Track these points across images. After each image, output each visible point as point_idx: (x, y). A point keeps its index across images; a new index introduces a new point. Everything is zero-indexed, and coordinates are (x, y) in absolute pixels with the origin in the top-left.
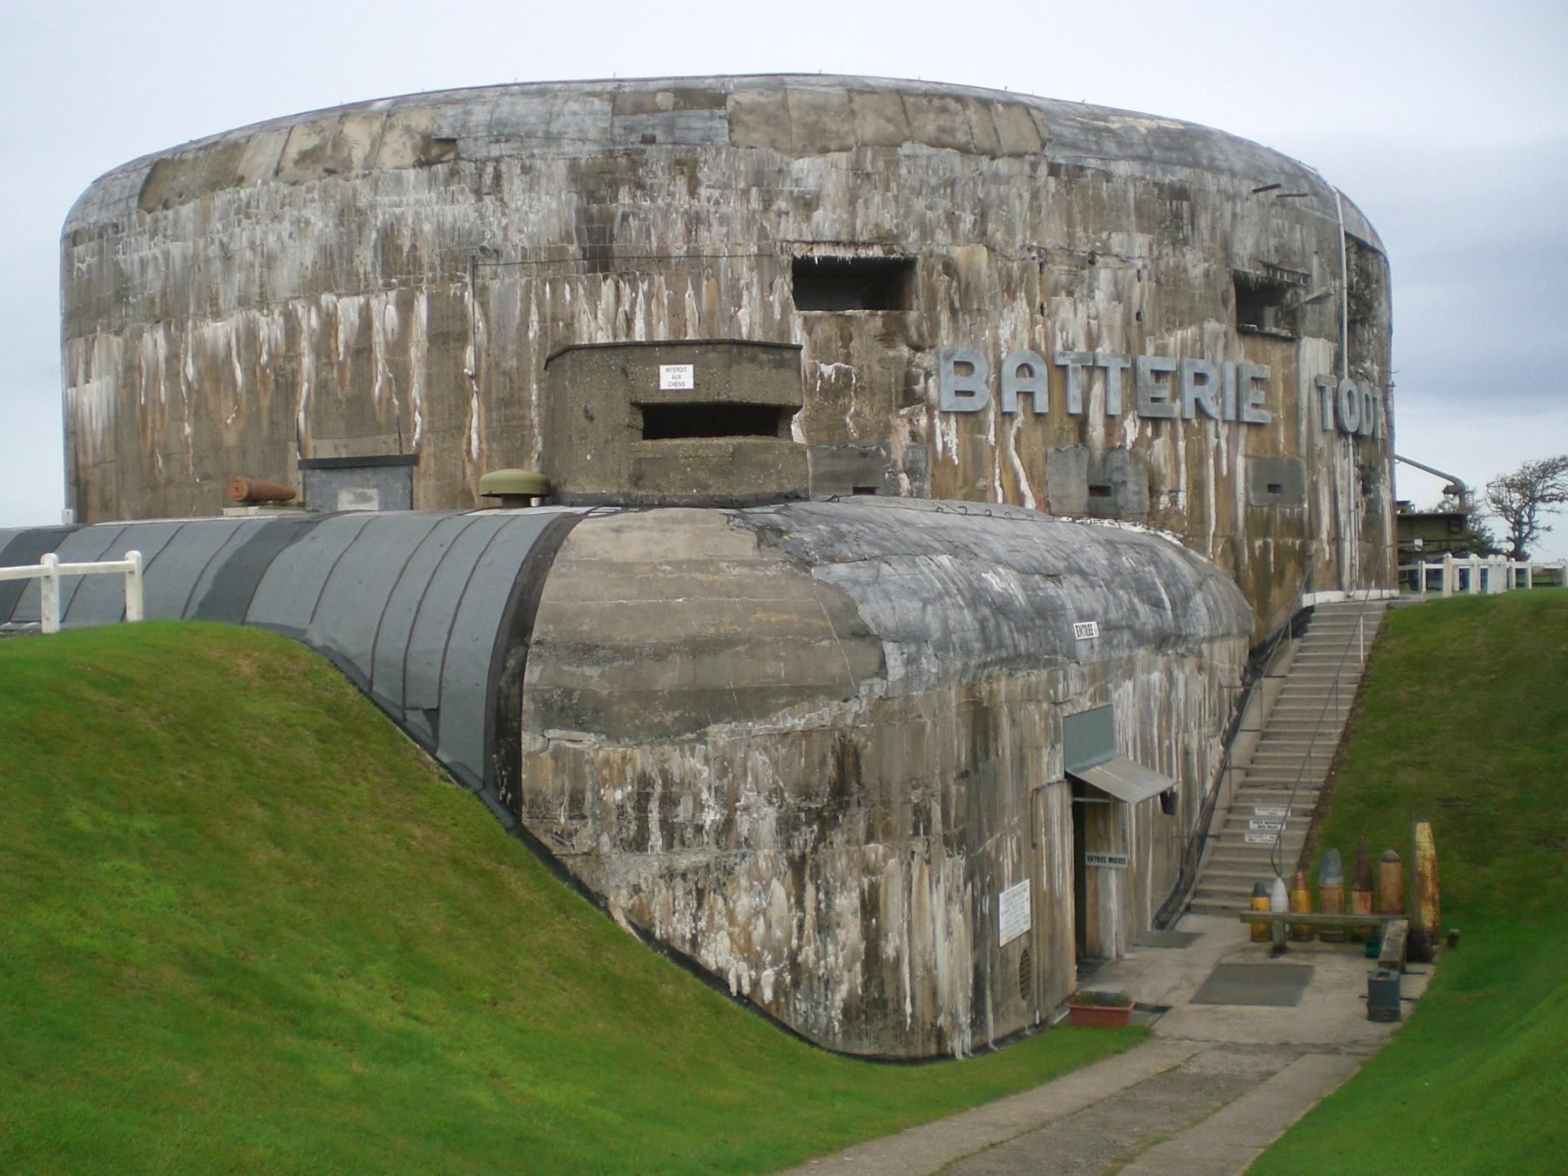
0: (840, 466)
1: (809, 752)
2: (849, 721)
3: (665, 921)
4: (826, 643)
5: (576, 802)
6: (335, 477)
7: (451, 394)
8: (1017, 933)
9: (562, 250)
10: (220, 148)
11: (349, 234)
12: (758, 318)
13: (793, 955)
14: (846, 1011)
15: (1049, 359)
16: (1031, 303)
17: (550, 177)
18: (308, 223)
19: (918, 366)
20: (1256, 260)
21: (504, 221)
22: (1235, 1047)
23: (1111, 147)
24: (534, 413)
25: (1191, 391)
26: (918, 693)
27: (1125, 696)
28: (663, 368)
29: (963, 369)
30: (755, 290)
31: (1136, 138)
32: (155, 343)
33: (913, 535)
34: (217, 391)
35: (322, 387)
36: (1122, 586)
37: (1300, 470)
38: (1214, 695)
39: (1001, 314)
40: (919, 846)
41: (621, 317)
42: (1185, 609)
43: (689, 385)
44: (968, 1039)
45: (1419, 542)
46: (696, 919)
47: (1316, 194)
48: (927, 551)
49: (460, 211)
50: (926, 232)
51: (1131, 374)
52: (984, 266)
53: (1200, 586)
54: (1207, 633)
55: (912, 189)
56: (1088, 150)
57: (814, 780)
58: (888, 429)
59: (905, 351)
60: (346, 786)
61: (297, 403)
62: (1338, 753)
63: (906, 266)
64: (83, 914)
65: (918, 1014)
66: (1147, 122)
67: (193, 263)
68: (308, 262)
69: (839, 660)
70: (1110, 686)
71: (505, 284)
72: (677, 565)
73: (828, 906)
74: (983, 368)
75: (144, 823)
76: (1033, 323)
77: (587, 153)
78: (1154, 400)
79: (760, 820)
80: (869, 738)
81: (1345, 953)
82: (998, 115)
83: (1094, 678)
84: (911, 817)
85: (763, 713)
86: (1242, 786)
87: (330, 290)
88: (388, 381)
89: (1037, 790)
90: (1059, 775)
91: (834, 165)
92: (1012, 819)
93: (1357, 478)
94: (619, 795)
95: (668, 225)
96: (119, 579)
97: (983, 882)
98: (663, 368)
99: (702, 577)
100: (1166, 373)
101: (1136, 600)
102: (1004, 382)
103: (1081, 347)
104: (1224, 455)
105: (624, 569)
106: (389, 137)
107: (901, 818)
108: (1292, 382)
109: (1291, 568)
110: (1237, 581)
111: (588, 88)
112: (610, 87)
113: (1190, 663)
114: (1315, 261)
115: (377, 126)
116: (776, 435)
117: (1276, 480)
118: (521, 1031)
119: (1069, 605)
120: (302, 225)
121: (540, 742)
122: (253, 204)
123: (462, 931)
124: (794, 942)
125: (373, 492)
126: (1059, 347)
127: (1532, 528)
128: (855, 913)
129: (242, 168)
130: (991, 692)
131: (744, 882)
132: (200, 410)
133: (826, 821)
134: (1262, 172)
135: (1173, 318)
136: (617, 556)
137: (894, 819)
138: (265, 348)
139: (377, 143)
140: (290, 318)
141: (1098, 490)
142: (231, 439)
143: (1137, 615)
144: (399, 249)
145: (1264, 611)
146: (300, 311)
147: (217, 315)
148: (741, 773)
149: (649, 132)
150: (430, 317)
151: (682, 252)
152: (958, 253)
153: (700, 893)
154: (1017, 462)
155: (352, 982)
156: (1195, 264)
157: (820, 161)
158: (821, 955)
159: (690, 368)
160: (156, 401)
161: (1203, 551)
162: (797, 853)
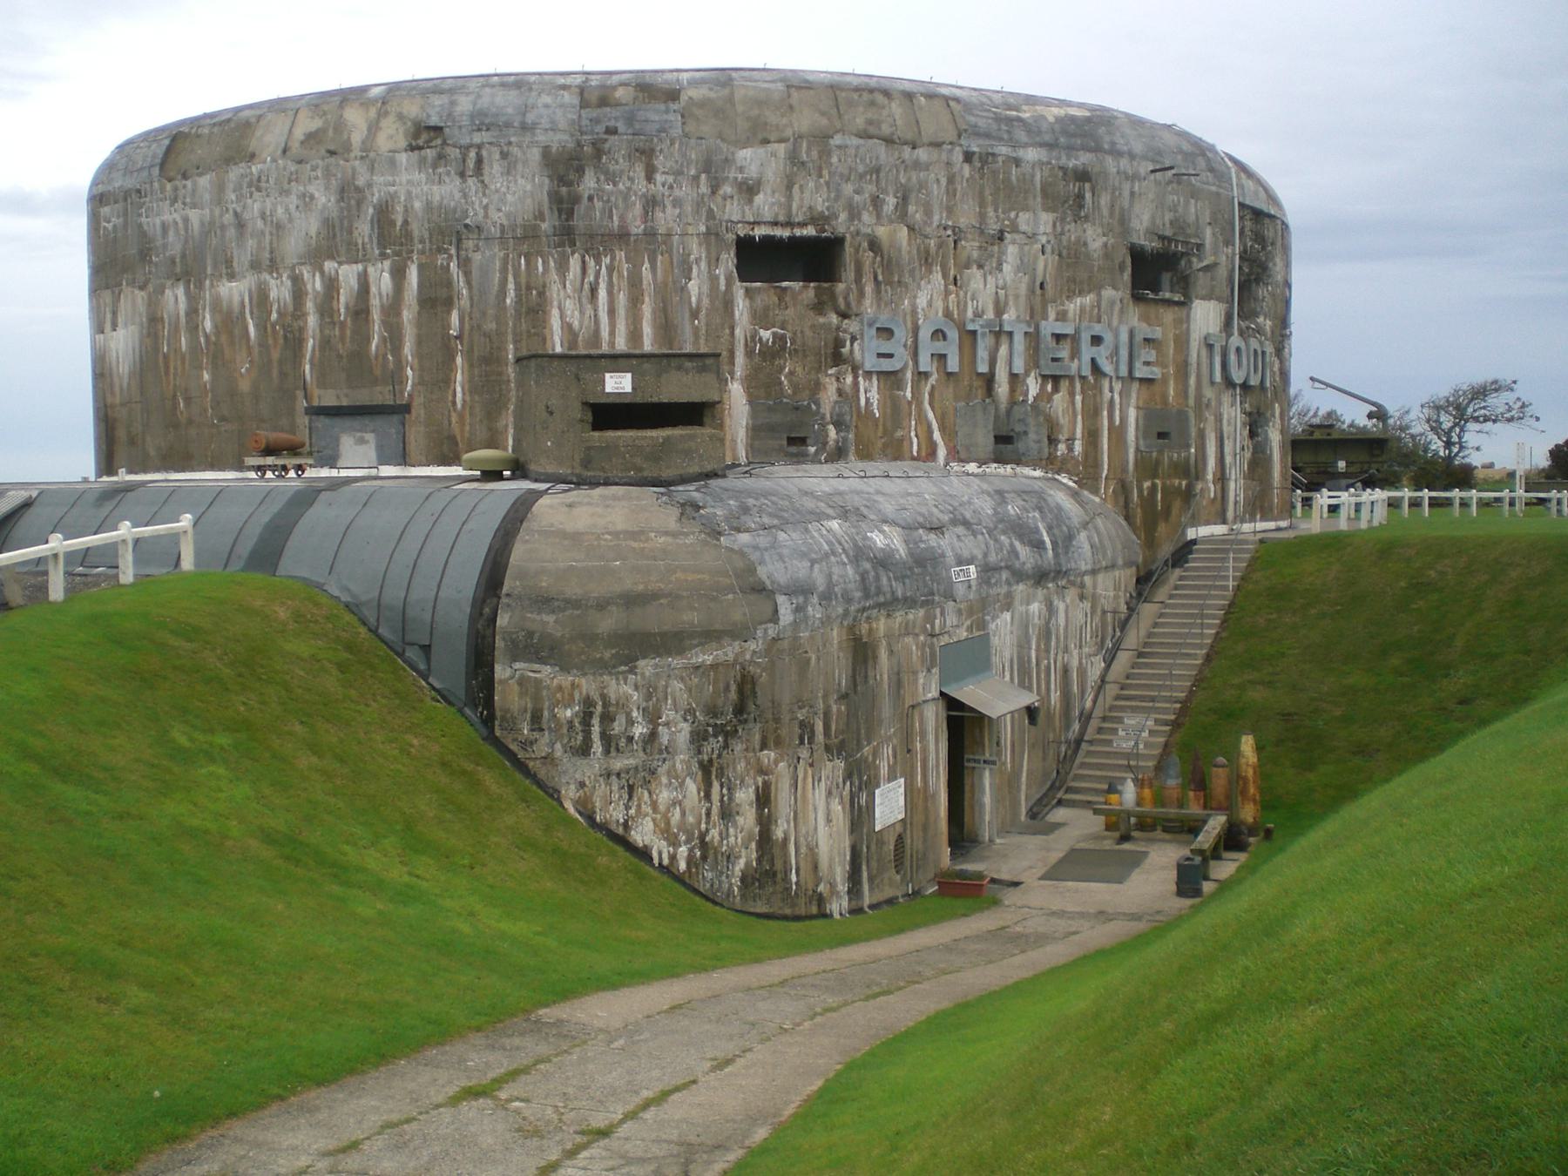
0: (777, 418)
1: (716, 681)
2: (748, 657)
3: (604, 809)
4: (730, 596)
5: (536, 718)
6: (338, 422)
7: (437, 354)
8: (892, 821)
9: (535, 228)
10: (233, 125)
11: (349, 209)
12: (705, 289)
13: (702, 836)
14: (743, 879)
15: (961, 326)
16: (945, 276)
17: (525, 162)
18: (312, 197)
19: (845, 331)
20: (1152, 233)
21: (485, 201)
22: (1061, 914)
23: (1021, 136)
24: (510, 370)
25: (1087, 352)
26: (804, 634)
27: (1003, 630)
28: (607, 375)
29: (885, 335)
30: (703, 265)
31: (1044, 126)
32: (176, 299)
33: (809, 504)
34: (232, 343)
35: (325, 344)
36: (1004, 532)
37: (1187, 419)
38: (1097, 619)
39: (919, 287)
40: (804, 753)
41: (586, 286)
42: (1067, 548)
43: (628, 389)
44: (845, 904)
45: (1342, 464)
46: (627, 808)
47: (1212, 170)
48: (820, 517)
49: (447, 190)
50: (854, 214)
51: (1033, 338)
52: (905, 243)
53: (1085, 525)
54: (1089, 567)
55: (841, 175)
56: (1001, 139)
57: (720, 702)
58: (817, 387)
59: (834, 319)
60: (361, 707)
61: (303, 356)
62: (1200, 672)
63: (836, 243)
64: (195, 805)
65: (802, 882)
66: (1055, 111)
67: (209, 228)
68: (313, 232)
69: (739, 610)
70: (988, 618)
71: (488, 257)
72: (616, 534)
73: (730, 799)
74: (901, 334)
75: (223, 740)
76: (947, 293)
77: (560, 140)
78: (1054, 360)
79: (678, 732)
80: (764, 670)
81: (1179, 842)
82: (921, 108)
83: (971, 612)
84: (797, 730)
85: (680, 651)
86: (1118, 698)
87: (332, 257)
88: (383, 340)
89: (913, 707)
90: (934, 693)
91: (774, 154)
92: (889, 730)
93: (1244, 424)
94: (569, 713)
95: (628, 206)
96: (175, 538)
97: (861, 780)
98: (607, 375)
99: (635, 545)
100: (1065, 336)
101: (1017, 544)
102: (920, 346)
103: (990, 315)
104: (1117, 407)
105: (575, 537)
106: (384, 123)
107: (790, 731)
108: (1182, 342)
109: (1177, 505)
110: (1127, 518)
111: (562, 81)
112: (579, 80)
113: (1071, 594)
114: (1208, 231)
115: (373, 112)
116: (701, 424)
117: (1165, 428)
118: (492, 887)
119: (949, 553)
120: (307, 200)
121: (508, 672)
122: (264, 178)
123: (448, 816)
124: (703, 826)
125: (370, 437)
126: (970, 314)
127: (1462, 448)
128: (751, 805)
129: (253, 145)
130: (871, 630)
131: (664, 780)
132: (218, 361)
133: (728, 734)
134: (1159, 153)
135: (1074, 287)
136: (569, 527)
137: (784, 732)
138: (275, 307)
139: (374, 128)
140: (297, 281)
141: (1003, 439)
142: (245, 386)
143: (1017, 556)
144: (393, 223)
145: (1150, 543)
146: (306, 276)
147: (232, 276)
148: (664, 699)
149: (612, 123)
150: (420, 285)
151: (640, 231)
152: (882, 232)
153: (631, 789)
154: (931, 415)
155: (372, 851)
156: (1095, 239)
157: (761, 151)
158: (724, 836)
159: (629, 375)
160: (177, 350)
161: (1096, 492)
162: (706, 758)
